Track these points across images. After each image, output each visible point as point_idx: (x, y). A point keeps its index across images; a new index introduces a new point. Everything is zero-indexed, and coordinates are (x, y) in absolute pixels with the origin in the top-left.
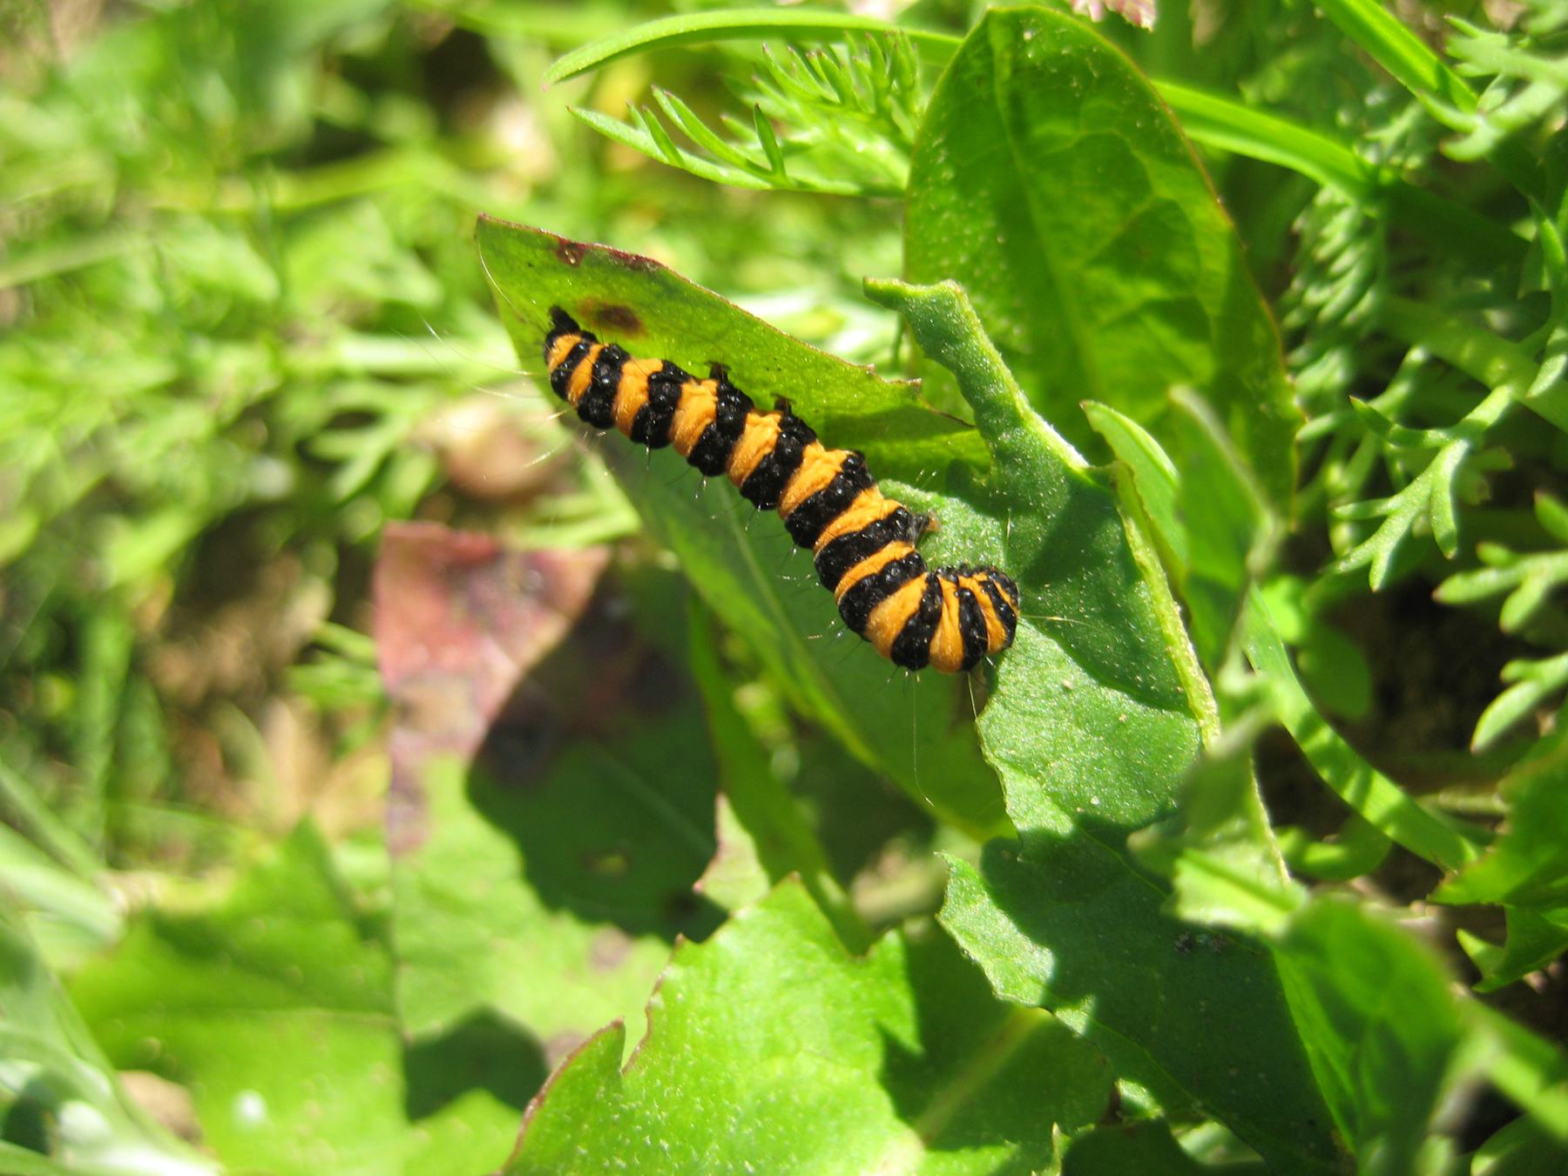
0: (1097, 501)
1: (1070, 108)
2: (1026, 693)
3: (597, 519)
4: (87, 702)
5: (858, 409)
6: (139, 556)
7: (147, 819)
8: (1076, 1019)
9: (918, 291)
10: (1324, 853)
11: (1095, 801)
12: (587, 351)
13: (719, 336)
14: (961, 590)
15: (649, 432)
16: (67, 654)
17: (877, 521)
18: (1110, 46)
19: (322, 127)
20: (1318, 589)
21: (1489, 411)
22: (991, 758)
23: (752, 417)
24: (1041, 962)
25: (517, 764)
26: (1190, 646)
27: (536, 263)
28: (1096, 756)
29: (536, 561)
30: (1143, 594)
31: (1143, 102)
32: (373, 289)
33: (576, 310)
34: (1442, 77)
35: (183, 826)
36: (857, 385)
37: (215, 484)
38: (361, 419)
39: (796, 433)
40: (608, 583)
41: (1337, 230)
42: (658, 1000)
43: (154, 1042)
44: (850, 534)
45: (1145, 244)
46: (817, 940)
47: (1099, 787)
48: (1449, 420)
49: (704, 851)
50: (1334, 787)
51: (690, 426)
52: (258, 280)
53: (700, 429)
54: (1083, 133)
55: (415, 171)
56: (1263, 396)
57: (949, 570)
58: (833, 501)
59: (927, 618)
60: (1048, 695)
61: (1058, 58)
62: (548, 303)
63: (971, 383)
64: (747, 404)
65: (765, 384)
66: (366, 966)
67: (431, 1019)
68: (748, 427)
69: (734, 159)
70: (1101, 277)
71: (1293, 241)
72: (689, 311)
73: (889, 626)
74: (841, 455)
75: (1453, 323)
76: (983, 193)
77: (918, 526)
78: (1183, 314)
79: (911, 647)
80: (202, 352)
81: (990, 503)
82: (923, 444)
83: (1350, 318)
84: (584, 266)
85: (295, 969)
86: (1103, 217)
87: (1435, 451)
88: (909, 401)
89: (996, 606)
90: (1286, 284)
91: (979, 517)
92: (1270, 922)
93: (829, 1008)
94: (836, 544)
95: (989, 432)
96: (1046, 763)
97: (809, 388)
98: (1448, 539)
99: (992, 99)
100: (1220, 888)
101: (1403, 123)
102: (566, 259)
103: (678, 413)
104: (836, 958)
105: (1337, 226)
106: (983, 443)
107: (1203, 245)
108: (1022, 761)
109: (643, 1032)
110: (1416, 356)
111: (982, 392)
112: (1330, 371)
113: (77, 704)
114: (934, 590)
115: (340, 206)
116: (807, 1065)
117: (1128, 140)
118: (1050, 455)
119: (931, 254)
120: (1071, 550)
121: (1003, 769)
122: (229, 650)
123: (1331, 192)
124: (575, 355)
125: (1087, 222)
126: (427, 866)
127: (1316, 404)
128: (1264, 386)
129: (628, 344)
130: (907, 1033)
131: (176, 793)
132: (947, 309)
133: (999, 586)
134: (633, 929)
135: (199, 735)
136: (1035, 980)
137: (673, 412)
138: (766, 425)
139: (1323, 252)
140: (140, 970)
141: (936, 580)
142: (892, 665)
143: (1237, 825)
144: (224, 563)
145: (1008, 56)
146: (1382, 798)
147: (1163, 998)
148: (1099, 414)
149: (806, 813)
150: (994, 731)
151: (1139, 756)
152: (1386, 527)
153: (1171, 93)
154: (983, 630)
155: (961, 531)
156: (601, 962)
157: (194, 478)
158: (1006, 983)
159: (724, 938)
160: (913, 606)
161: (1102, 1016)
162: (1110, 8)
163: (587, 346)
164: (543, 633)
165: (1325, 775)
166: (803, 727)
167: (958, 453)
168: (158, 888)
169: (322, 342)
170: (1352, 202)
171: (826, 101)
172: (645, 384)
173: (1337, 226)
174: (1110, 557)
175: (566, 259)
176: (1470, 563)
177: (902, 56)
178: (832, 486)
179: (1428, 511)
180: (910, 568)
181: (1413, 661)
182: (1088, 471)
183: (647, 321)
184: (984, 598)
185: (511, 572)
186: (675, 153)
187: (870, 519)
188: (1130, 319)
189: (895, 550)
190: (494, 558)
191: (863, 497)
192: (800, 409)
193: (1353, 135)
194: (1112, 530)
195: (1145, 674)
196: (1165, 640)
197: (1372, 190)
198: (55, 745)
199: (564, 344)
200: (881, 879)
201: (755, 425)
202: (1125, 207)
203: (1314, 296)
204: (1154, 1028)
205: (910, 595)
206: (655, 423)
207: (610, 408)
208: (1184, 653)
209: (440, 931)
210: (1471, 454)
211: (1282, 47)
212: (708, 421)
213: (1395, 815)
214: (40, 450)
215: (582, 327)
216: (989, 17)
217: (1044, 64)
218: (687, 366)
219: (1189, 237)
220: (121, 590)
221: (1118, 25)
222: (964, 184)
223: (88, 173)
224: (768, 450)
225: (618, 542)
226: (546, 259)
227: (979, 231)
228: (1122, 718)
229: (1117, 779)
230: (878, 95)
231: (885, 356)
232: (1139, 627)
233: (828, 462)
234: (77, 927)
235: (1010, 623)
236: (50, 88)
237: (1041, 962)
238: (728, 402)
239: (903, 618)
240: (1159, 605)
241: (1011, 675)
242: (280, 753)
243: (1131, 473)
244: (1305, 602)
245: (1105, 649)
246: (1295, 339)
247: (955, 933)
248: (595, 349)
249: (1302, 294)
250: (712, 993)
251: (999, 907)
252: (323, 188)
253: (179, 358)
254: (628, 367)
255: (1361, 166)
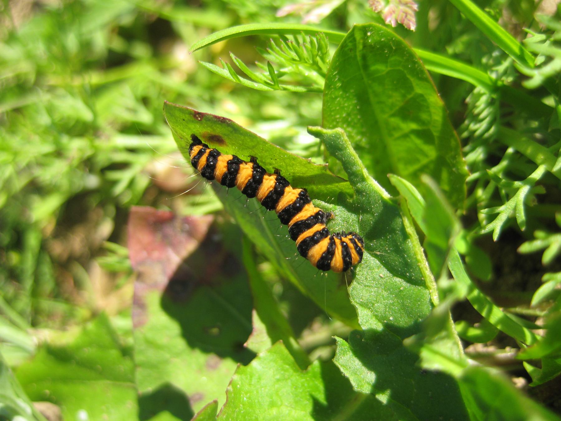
0: (393, 209)
1: (384, 60)
2: (366, 279)
3: (204, 208)
4: (27, 261)
5: (305, 174)
6: (43, 211)
7: (46, 304)
8: (383, 398)
9: (327, 132)
10: (474, 332)
11: (391, 318)
12: (205, 152)
13: (254, 147)
14: (342, 242)
15: (228, 182)
16: (18, 244)
17: (312, 216)
18: (399, 37)
19: (111, 52)
20: (472, 235)
21: (537, 174)
22: (353, 302)
23: (266, 177)
24: (371, 377)
25: (179, 294)
26: (427, 263)
27: (186, 119)
28: (391, 301)
29: (187, 220)
30: (410, 244)
31: (411, 57)
32: (128, 117)
33: (201, 136)
34: (521, 50)
35: (60, 307)
36: (304, 165)
37: (71, 183)
38: (122, 166)
39: (282, 182)
40: (213, 229)
41: (482, 102)
42: (230, 388)
43: (47, 391)
44: (301, 221)
45: (411, 109)
46: (289, 365)
47: (392, 313)
48: (522, 177)
49: (248, 331)
50: (479, 312)
51: (243, 180)
52: (86, 115)
53: (246, 181)
54: (389, 69)
55: (142, 73)
56: (454, 166)
57: (338, 234)
58: (295, 208)
59: (330, 253)
60: (374, 279)
61: (380, 42)
62: (190, 133)
63: (347, 165)
64: (264, 172)
65: (271, 164)
66: (125, 366)
67: (149, 387)
68: (264, 180)
69: (260, 81)
70: (395, 121)
71: (464, 105)
72: (242, 137)
73: (316, 256)
74: (299, 191)
75: (524, 139)
76: (352, 91)
77: (327, 217)
78: (425, 135)
79: (324, 263)
80: (65, 140)
81: (354, 209)
82: (329, 186)
83: (486, 135)
84: (204, 121)
85: (99, 366)
86: (396, 99)
87: (517, 189)
88: (324, 171)
89: (356, 248)
90: (463, 121)
91: (349, 214)
92: (456, 372)
93: (293, 389)
94: (296, 224)
95: (353, 183)
96: (373, 304)
97: (287, 166)
98: (522, 223)
99: (355, 57)
100: (438, 358)
101: (505, 64)
102: (197, 118)
103: (238, 175)
104: (295, 371)
105: (482, 103)
106: (351, 186)
107: (432, 110)
108: (365, 304)
109: (225, 401)
110: (510, 150)
111: (351, 169)
112: (478, 155)
113: (22, 261)
114: (332, 243)
115: (118, 82)
116: (285, 410)
117: (406, 72)
118: (375, 192)
119: (332, 114)
120: (383, 227)
121: (357, 306)
122: (77, 242)
123: (479, 89)
124: (201, 153)
125: (390, 101)
126: (145, 331)
127: (473, 167)
128: (455, 162)
129: (220, 148)
130: (321, 397)
131: (57, 294)
132: (338, 138)
133: (356, 240)
134: (222, 355)
135: (67, 270)
136: (368, 383)
137: (236, 174)
138: (271, 180)
139: (476, 111)
140: (42, 366)
141: (333, 239)
142: (317, 269)
143: (443, 334)
144: (75, 211)
145: (362, 41)
146: (497, 314)
147: (415, 390)
148: (394, 179)
149: (284, 309)
150: (355, 292)
151: (407, 302)
152: (499, 217)
153: (420, 53)
154: (350, 258)
155: (342, 218)
156: (211, 367)
157: (65, 184)
158: (358, 385)
159: (255, 363)
160: (324, 249)
161: (393, 397)
162: (399, 22)
163: (205, 150)
164: (190, 246)
165: (476, 307)
166: (284, 281)
167: (342, 190)
168: (48, 335)
169: (108, 138)
170: (487, 92)
171: (294, 60)
172: (226, 164)
173: (482, 103)
174: (397, 230)
175: (197, 118)
176: (532, 238)
177: (322, 42)
178: (295, 203)
179: (515, 209)
180: (324, 234)
181: (507, 268)
182: (390, 199)
183: (227, 141)
184: (351, 245)
185: (178, 224)
186: (238, 78)
187: (309, 215)
188: (405, 136)
189: (318, 227)
190: (172, 218)
191: (306, 207)
192: (283, 174)
193: (487, 68)
194: (399, 220)
195: (410, 273)
196: (418, 261)
197: (495, 88)
198: (14, 275)
199: (196, 149)
200: (313, 332)
201: (267, 179)
202: (404, 96)
203: (473, 127)
204: (412, 402)
205: (324, 244)
206: (229, 179)
207: (213, 173)
208: (424, 265)
209: (151, 355)
210: (530, 192)
211: (462, 33)
212: (250, 178)
213: (501, 321)
214: (9, 171)
215: (203, 142)
216: (355, 27)
217: (375, 44)
218: (241, 157)
219: (428, 107)
220: (36, 223)
221: (401, 28)
222: (344, 88)
223: (26, 68)
224: (271, 189)
225: (216, 213)
226: (189, 118)
227: (350, 104)
228: (402, 289)
229: (399, 311)
230: (313, 57)
231: (315, 149)
232: (408, 256)
233: (294, 193)
234: (20, 348)
235: (360, 254)
236: (11, 38)
237: (371, 377)
238: (257, 171)
239: (321, 253)
240: (415, 247)
241: (361, 272)
242: (95, 280)
243: (406, 201)
244: (468, 238)
245: (395, 263)
246: (465, 142)
247: (339, 366)
248: (208, 151)
249: (468, 126)
250: (250, 385)
251: (356, 357)
252: (113, 76)
253: (57, 143)
254: (220, 158)
255: (491, 79)
